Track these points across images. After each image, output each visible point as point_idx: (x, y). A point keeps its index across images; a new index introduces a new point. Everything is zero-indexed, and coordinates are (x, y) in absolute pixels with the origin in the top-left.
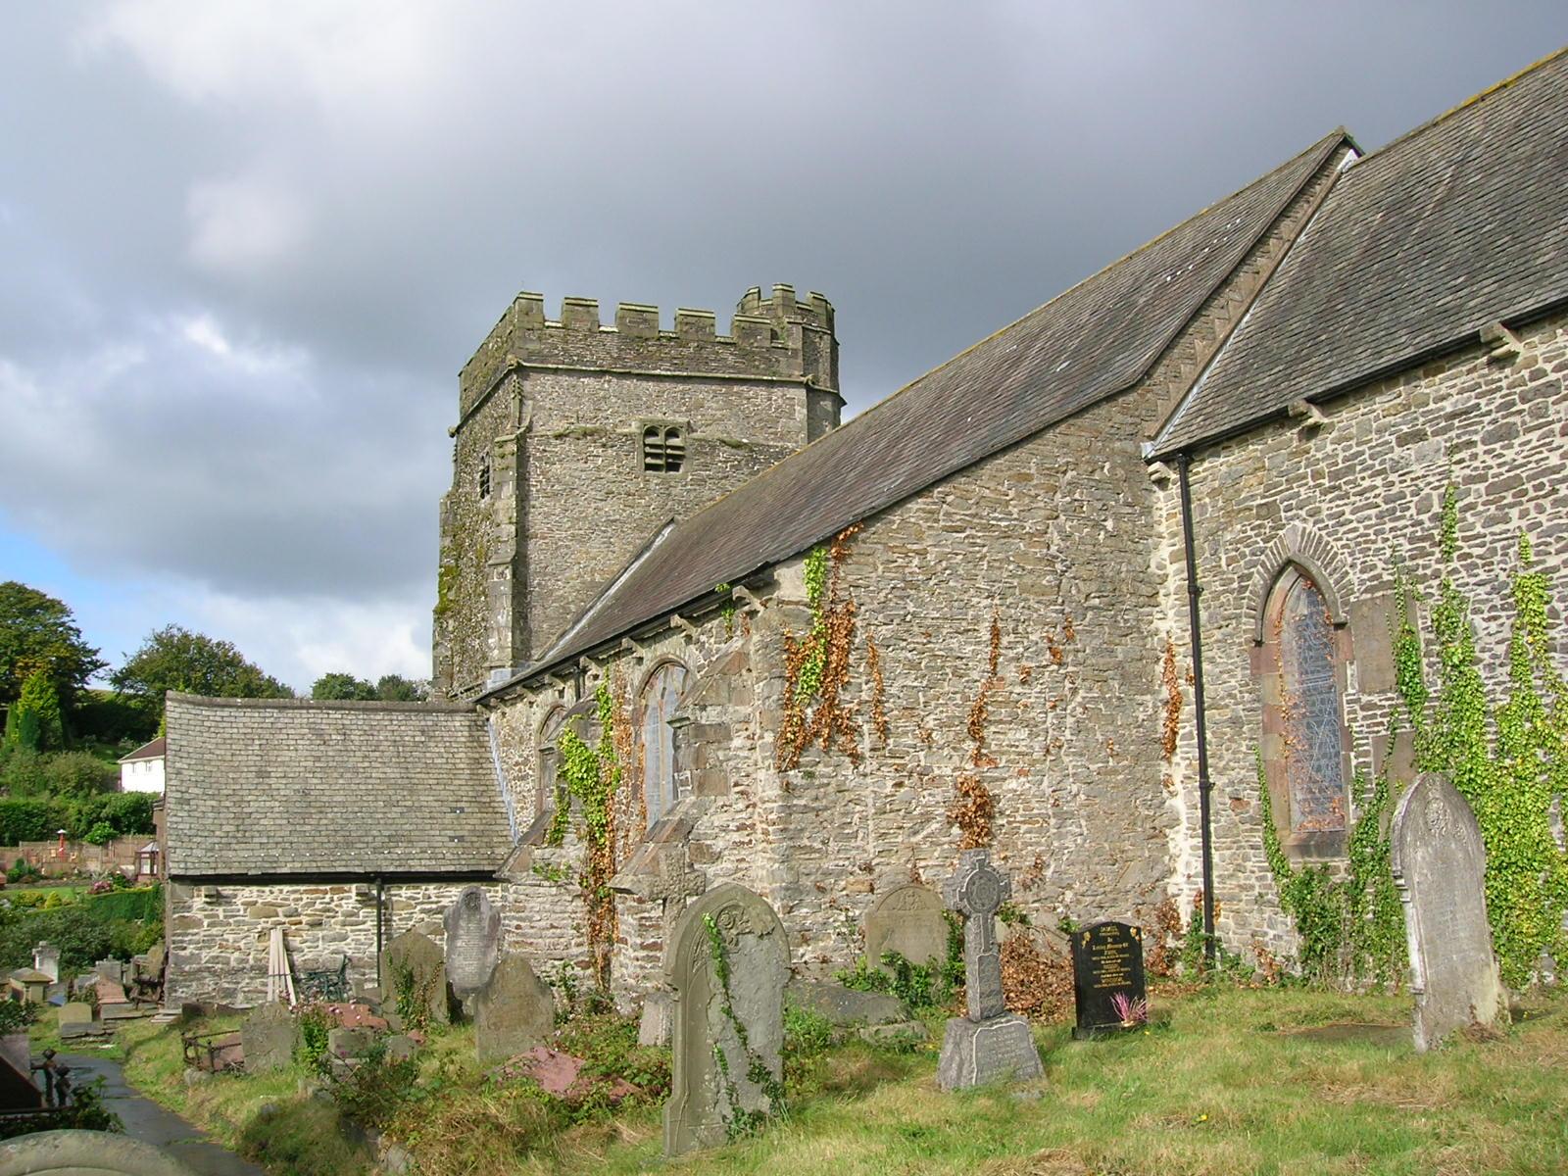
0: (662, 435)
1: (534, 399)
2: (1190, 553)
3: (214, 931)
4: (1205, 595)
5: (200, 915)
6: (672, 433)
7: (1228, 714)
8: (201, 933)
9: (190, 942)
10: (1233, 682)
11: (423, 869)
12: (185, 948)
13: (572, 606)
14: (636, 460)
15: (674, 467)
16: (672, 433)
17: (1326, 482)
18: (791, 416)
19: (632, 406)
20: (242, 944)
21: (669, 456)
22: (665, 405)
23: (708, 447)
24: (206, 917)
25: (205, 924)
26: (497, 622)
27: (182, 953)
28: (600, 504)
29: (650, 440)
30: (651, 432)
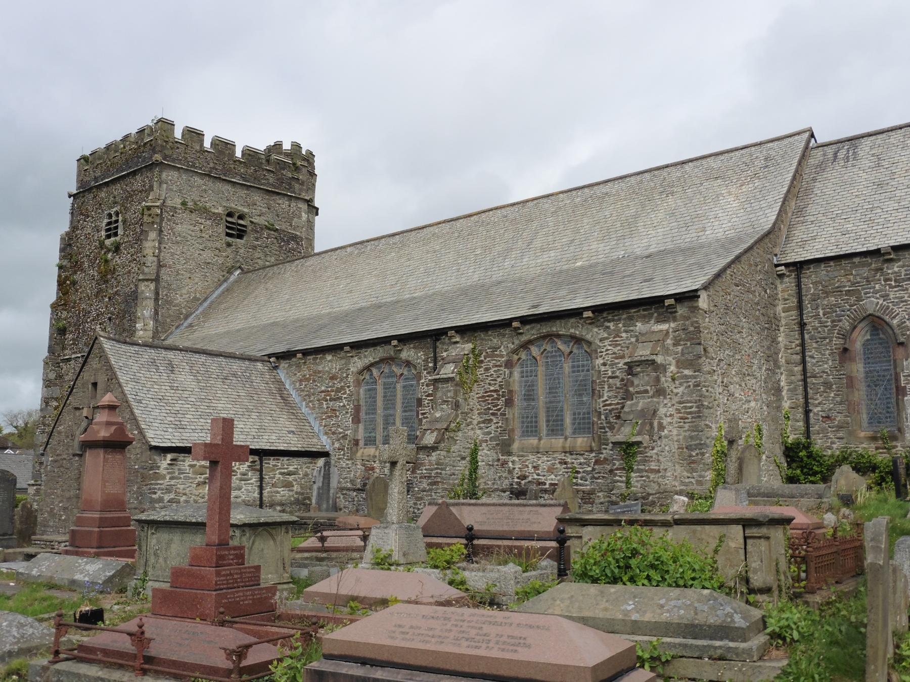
0: (236, 217)
1: (167, 183)
2: (800, 307)
3: (173, 482)
4: (808, 327)
5: (165, 472)
6: (241, 217)
7: (822, 380)
8: (166, 482)
9: (159, 489)
10: (826, 366)
11: (282, 448)
12: (155, 493)
13: (184, 310)
14: (221, 229)
15: (240, 237)
16: (241, 217)
17: (893, 283)
18: (300, 217)
19: (221, 198)
20: (187, 491)
21: (239, 230)
22: (237, 200)
23: (259, 229)
24: (169, 473)
25: (168, 477)
26: (143, 314)
27: (154, 496)
28: (201, 252)
29: (229, 219)
30: (230, 215)
